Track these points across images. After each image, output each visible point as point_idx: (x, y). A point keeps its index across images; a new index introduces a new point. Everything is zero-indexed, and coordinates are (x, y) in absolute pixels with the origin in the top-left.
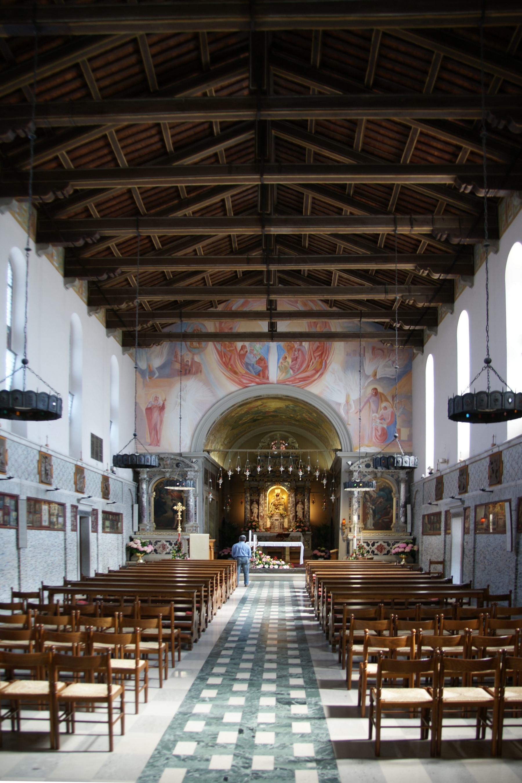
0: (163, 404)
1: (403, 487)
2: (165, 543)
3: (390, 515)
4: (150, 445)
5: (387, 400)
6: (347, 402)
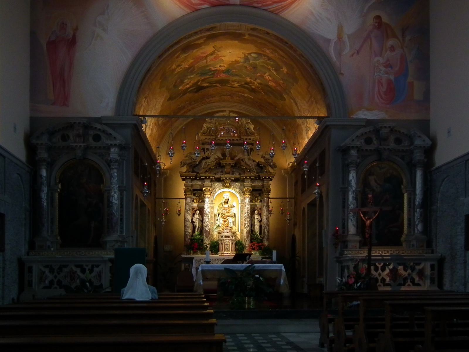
0: (74, 36)
1: (419, 174)
2: (74, 269)
4: (54, 104)
5: (395, 36)
6: (340, 37)
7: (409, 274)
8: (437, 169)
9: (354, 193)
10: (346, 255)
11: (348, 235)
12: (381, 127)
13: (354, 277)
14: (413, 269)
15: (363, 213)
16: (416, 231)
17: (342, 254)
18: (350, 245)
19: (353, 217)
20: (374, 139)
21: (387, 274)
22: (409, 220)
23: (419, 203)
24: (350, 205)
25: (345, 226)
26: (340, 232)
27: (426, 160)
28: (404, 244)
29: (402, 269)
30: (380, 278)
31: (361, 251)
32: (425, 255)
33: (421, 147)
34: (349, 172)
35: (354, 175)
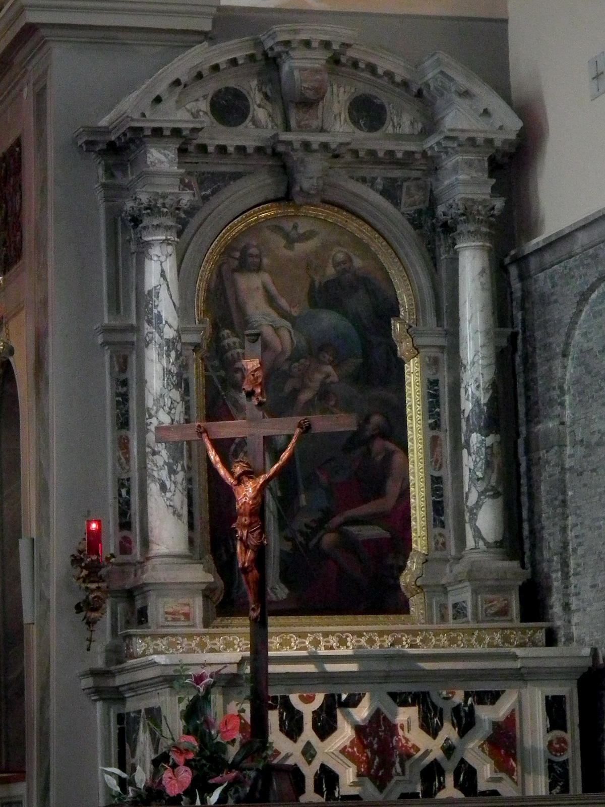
1: (471, 266)
3: (392, 488)
7: (449, 750)
8: (550, 245)
9: (168, 356)
10: (143, 659)
11: (148, 559)
12: (287, 43)
13: (187, 763)
14: (465, 722)
15: (221, 446)
16: (470, 542)
17: (118, 654)
18: (159, 608)
19: (172, 472)
20: (255, 97)
21: (345, 747)
22: (435, 484)
23: (477, 403)
24: (153, 413)
25: (129, 517)
26: (110, 546)
27: (499, 204)
28: (416, 604)
29: (416, 724)
30: (310, 772)
31: (213, 636)
32: (519, 652)
33: (472, 141)
34: (142, 250)
35: (170, 266)
